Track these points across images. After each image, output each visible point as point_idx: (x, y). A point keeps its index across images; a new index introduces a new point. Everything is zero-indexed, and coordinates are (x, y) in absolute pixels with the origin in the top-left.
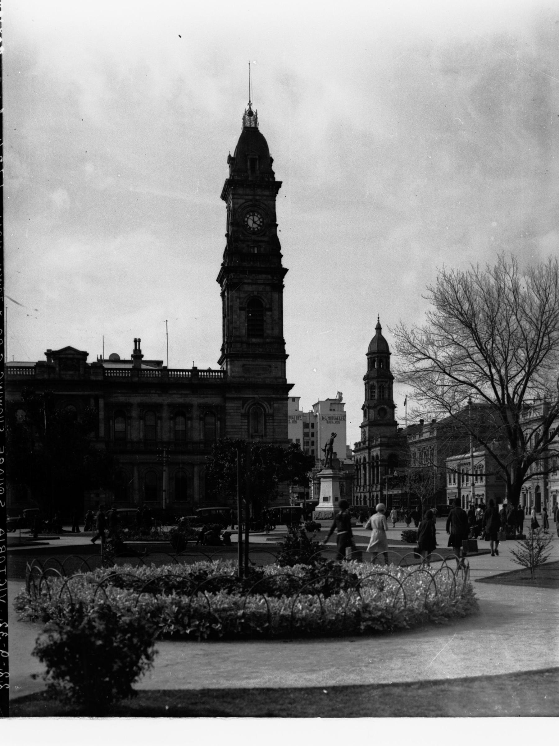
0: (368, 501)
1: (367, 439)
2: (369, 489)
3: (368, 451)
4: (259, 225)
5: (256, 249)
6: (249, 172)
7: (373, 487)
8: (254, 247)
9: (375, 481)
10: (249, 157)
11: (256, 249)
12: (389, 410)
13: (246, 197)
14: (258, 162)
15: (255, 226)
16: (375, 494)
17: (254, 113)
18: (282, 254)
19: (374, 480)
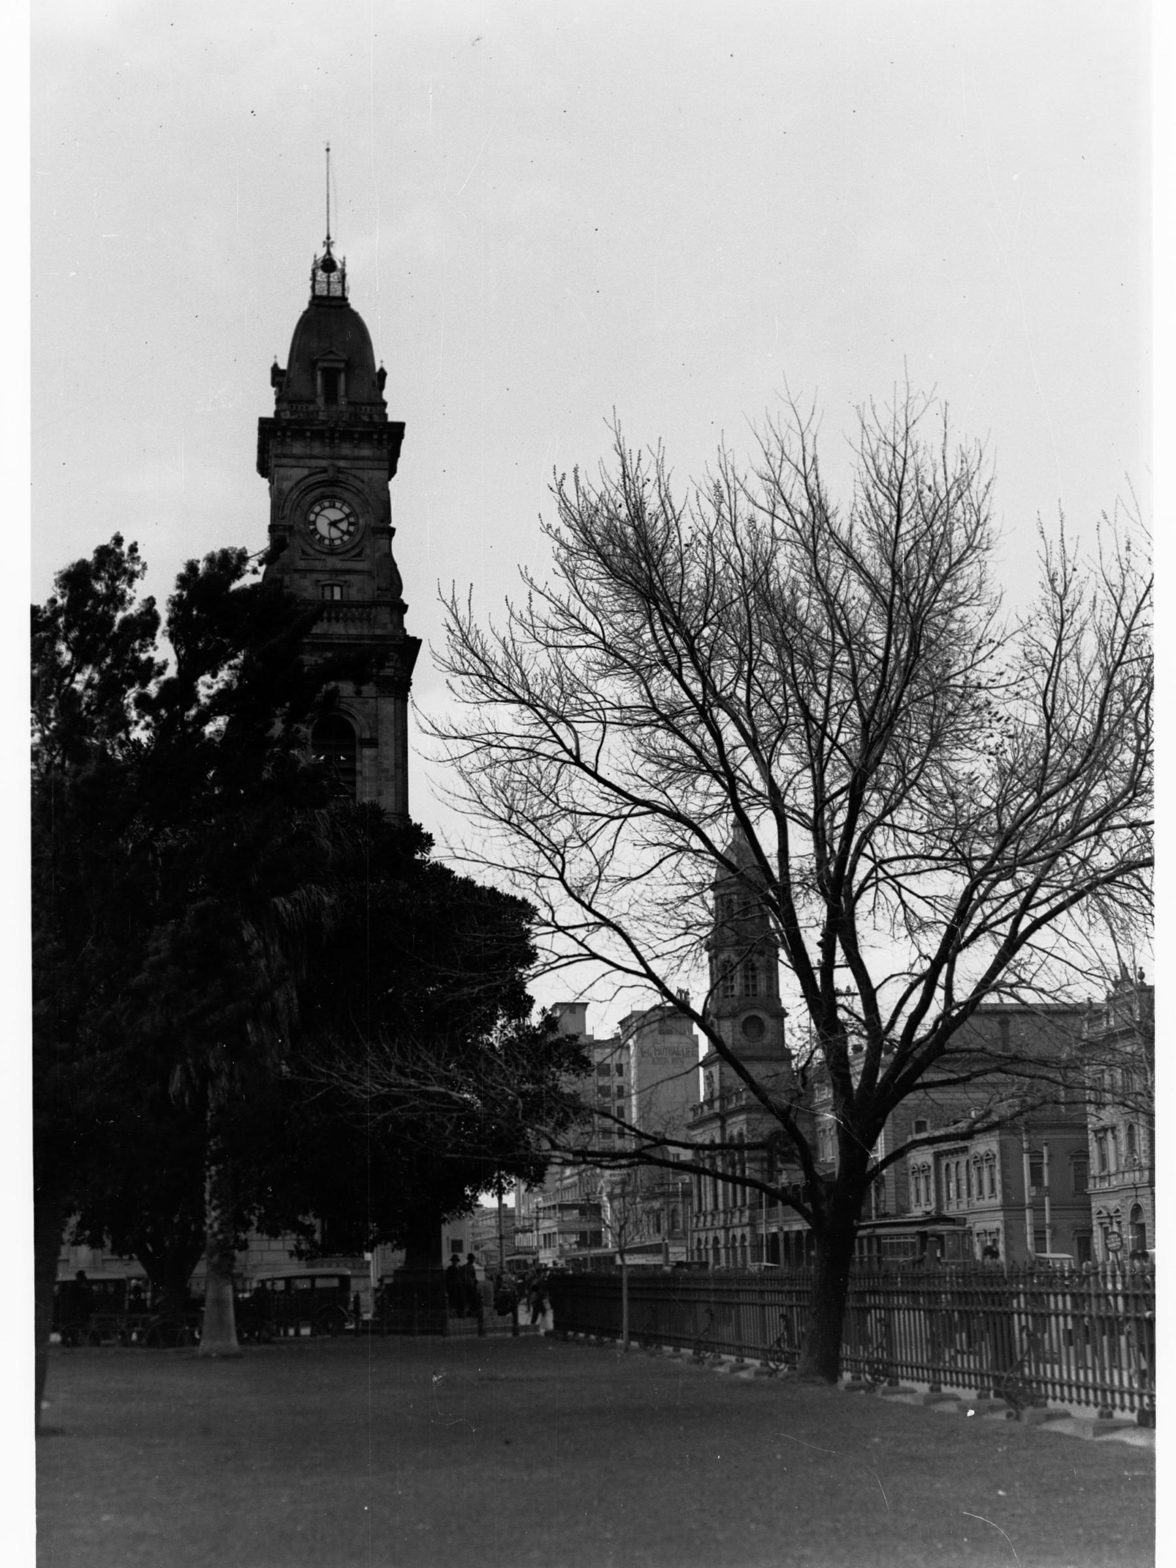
0: (723, 1251)
1: (717, 1094)
2: (725, 1221)
3: (719, 1123)
4: (348, 533)
5: (337, 590)
6: (320, 401)
7: (733, 1214)
8: (332, 586)
9: (739, 1203)
10: (320, 364)
11: (337, 590)
12: (769, 1022)
13: (313, 463)
14: (343, 376)
15: (335, 533)
16: (738, 1232)
17: (339, 266)
18: (406, 602)
19: (735, 1201)
